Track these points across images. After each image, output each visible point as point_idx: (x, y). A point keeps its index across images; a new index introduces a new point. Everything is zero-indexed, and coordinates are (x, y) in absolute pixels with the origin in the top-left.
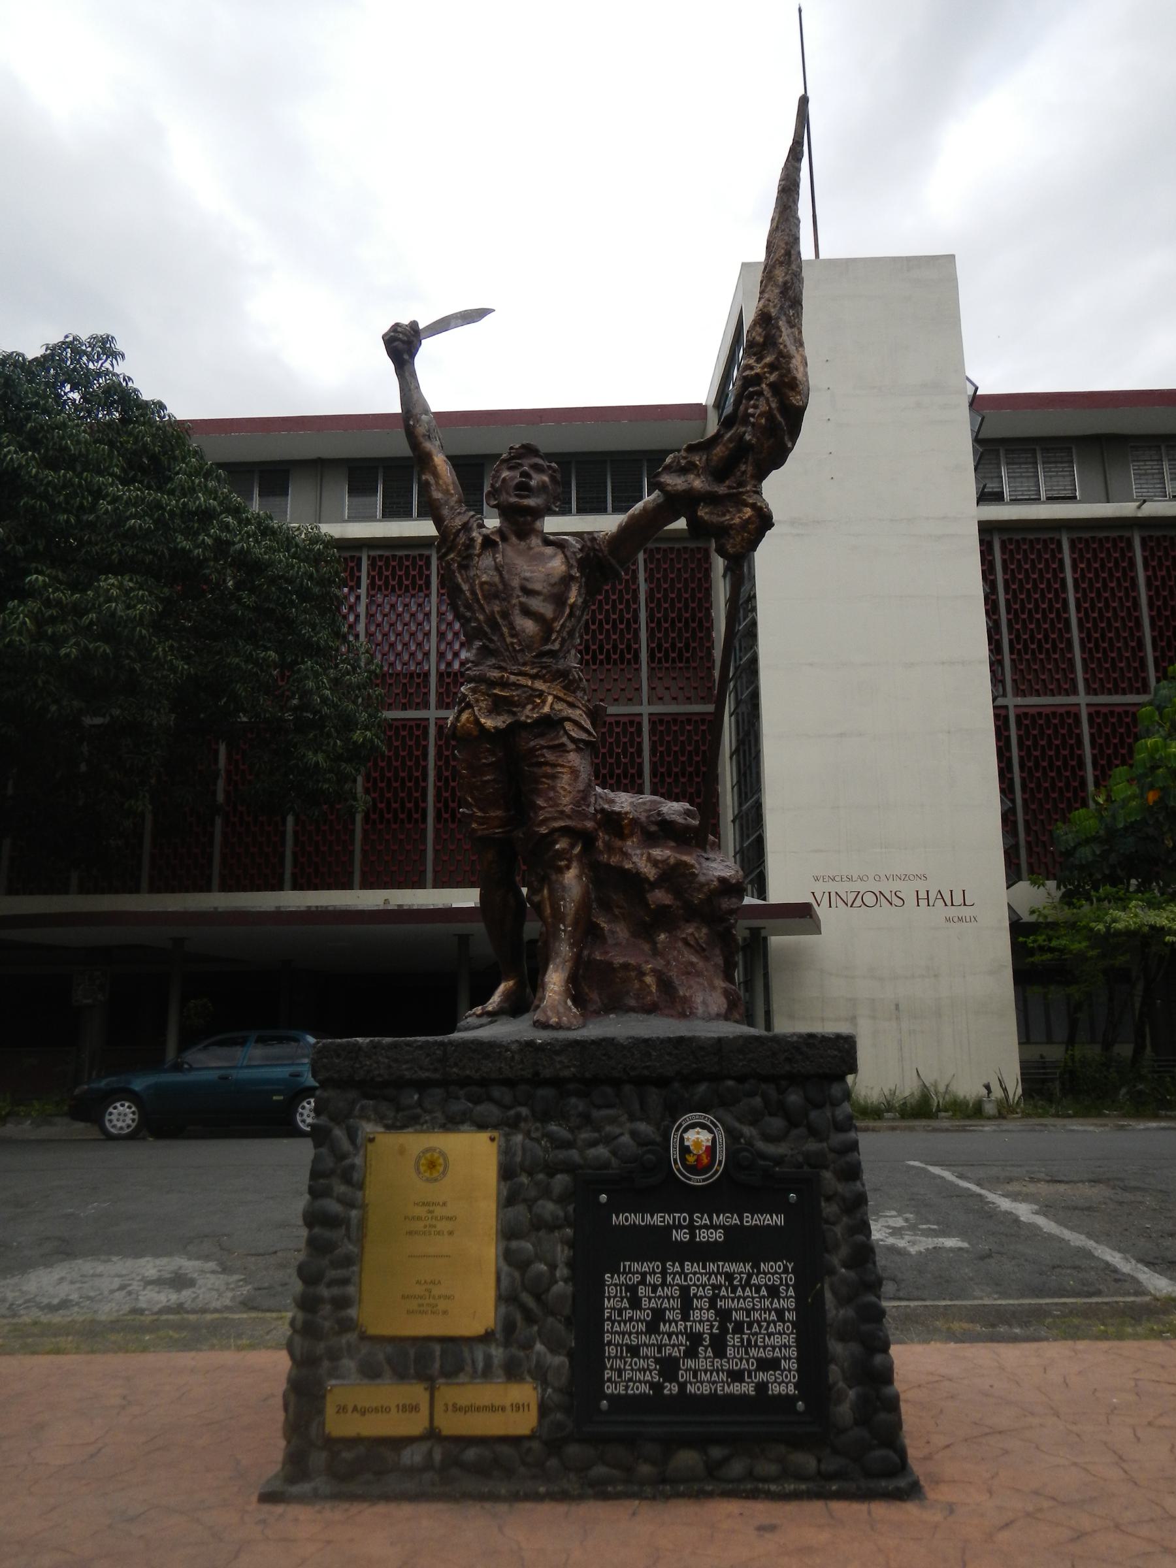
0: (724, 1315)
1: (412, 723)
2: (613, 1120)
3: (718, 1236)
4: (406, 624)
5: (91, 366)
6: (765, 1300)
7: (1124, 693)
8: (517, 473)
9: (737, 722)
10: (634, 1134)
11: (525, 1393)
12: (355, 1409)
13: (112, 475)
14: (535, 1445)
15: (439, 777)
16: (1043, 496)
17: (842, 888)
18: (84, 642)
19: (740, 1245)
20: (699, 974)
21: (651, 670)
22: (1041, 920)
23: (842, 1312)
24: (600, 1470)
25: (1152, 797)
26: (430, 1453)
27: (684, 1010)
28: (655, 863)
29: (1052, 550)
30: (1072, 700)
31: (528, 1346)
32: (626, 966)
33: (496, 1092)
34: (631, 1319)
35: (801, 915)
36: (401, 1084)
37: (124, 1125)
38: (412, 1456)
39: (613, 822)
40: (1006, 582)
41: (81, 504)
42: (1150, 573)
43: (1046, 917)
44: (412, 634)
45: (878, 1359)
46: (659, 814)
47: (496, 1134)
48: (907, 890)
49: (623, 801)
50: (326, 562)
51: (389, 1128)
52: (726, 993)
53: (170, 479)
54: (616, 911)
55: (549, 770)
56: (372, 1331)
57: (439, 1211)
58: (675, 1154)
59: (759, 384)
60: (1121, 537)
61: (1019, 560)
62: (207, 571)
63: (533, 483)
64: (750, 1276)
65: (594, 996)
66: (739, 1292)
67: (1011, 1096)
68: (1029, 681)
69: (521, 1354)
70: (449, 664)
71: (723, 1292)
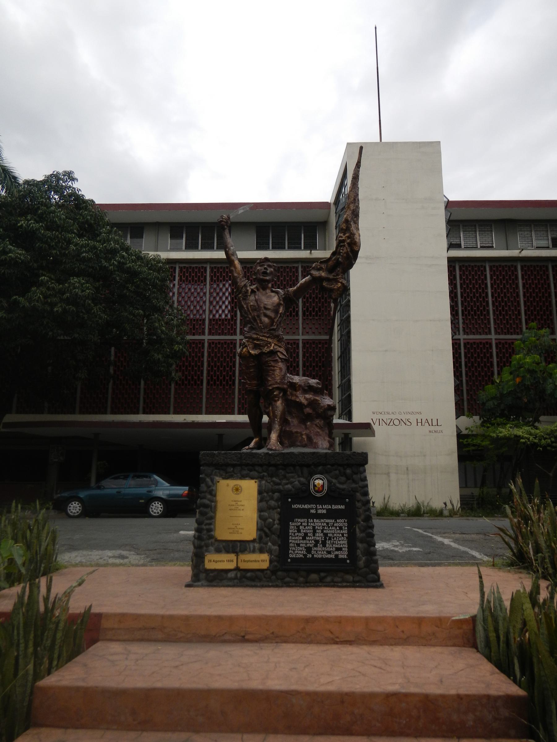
0: (326, 535)
1: (197, 341)
2: (293, 477)
3: (324, 511)
4: (195, 297)
5: (64, 184)
6: (338, 532)
7: (512, 334)
8: (262, 268)
9: (341, 344)
10: (299, 481)
11: (265, 557)
12: (214, 561)
13: (74, 233)
14: (268, 572)
15: (209, 365)
16: (479, 246)
17: (385, 417)
18: (64, 305)
19: (331, 514)
20: (320, 435)
21: (303, 320)
22: (470, 433)
23: (361, 535)
24: (287, 579)
25: (518, 380)
26: (236, 574)
27: (315, 446)
28: (307, 399)
29: (482, 270)
30: (489, 337)
31: (266, 544)
32: (297, 432)
33: (257, 468)
34: (298, 536)
35: (366, 428)
36: (227, 465)
37: (76, 511)
38: (231, 575)
39: (293, 386)
40: (461, 284)
41: (62, 246)
42: (524, 281)
43: (472, 431)
44: (198, 302)
45: (372, 548)
46: (308, 383)
47: (257, 481)
48: (413, 418)
49: (296, 379)
50: (163, 271)
51: (224, 478)
52: (329, 442)
53: (98, 235)
54: (294, 415)
55: (272, 368)
56: (219, 538)
57: (239, 503)
58: (312, 487)
59: (344, 243)
60: (512, 265)
61: (467, 275)
62: (115, 276)
63: (268, 271)
64: (334, 523)
65: (286, 442)
66: (331, 528)
67: (455, 507)
68: (470, 328)
69: (264, 546)
70: (214, 316)
71: (326, 528)
